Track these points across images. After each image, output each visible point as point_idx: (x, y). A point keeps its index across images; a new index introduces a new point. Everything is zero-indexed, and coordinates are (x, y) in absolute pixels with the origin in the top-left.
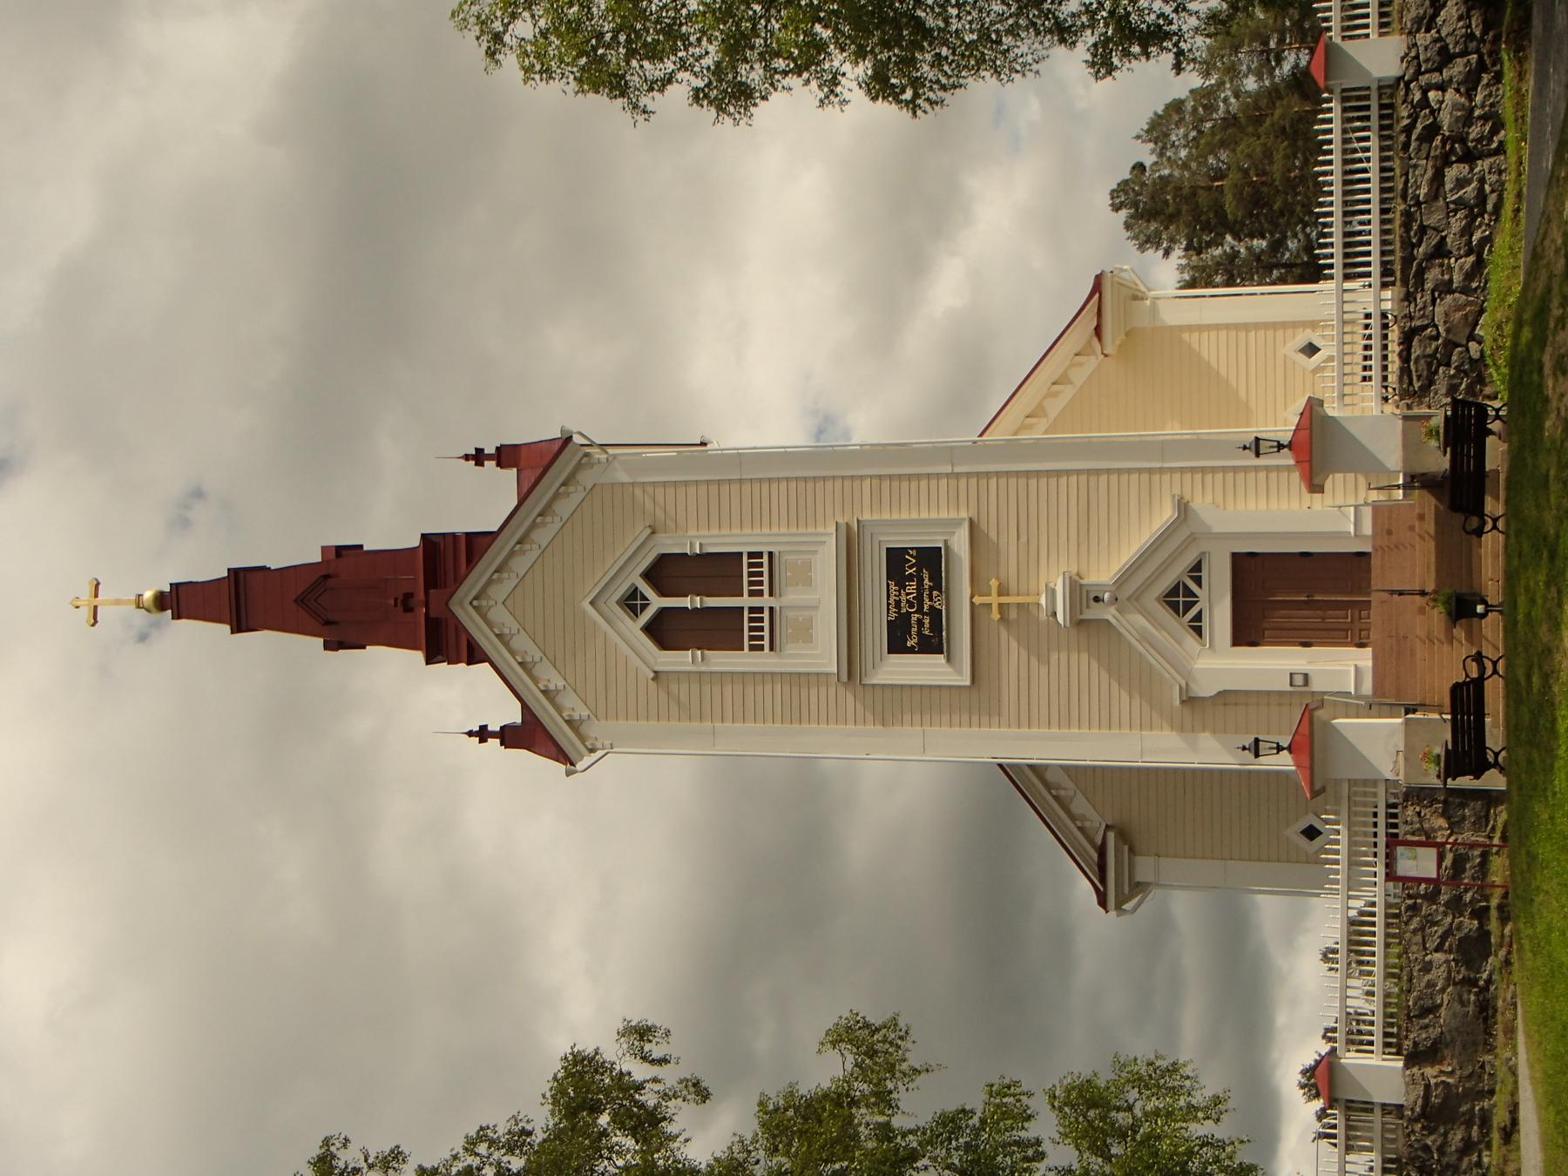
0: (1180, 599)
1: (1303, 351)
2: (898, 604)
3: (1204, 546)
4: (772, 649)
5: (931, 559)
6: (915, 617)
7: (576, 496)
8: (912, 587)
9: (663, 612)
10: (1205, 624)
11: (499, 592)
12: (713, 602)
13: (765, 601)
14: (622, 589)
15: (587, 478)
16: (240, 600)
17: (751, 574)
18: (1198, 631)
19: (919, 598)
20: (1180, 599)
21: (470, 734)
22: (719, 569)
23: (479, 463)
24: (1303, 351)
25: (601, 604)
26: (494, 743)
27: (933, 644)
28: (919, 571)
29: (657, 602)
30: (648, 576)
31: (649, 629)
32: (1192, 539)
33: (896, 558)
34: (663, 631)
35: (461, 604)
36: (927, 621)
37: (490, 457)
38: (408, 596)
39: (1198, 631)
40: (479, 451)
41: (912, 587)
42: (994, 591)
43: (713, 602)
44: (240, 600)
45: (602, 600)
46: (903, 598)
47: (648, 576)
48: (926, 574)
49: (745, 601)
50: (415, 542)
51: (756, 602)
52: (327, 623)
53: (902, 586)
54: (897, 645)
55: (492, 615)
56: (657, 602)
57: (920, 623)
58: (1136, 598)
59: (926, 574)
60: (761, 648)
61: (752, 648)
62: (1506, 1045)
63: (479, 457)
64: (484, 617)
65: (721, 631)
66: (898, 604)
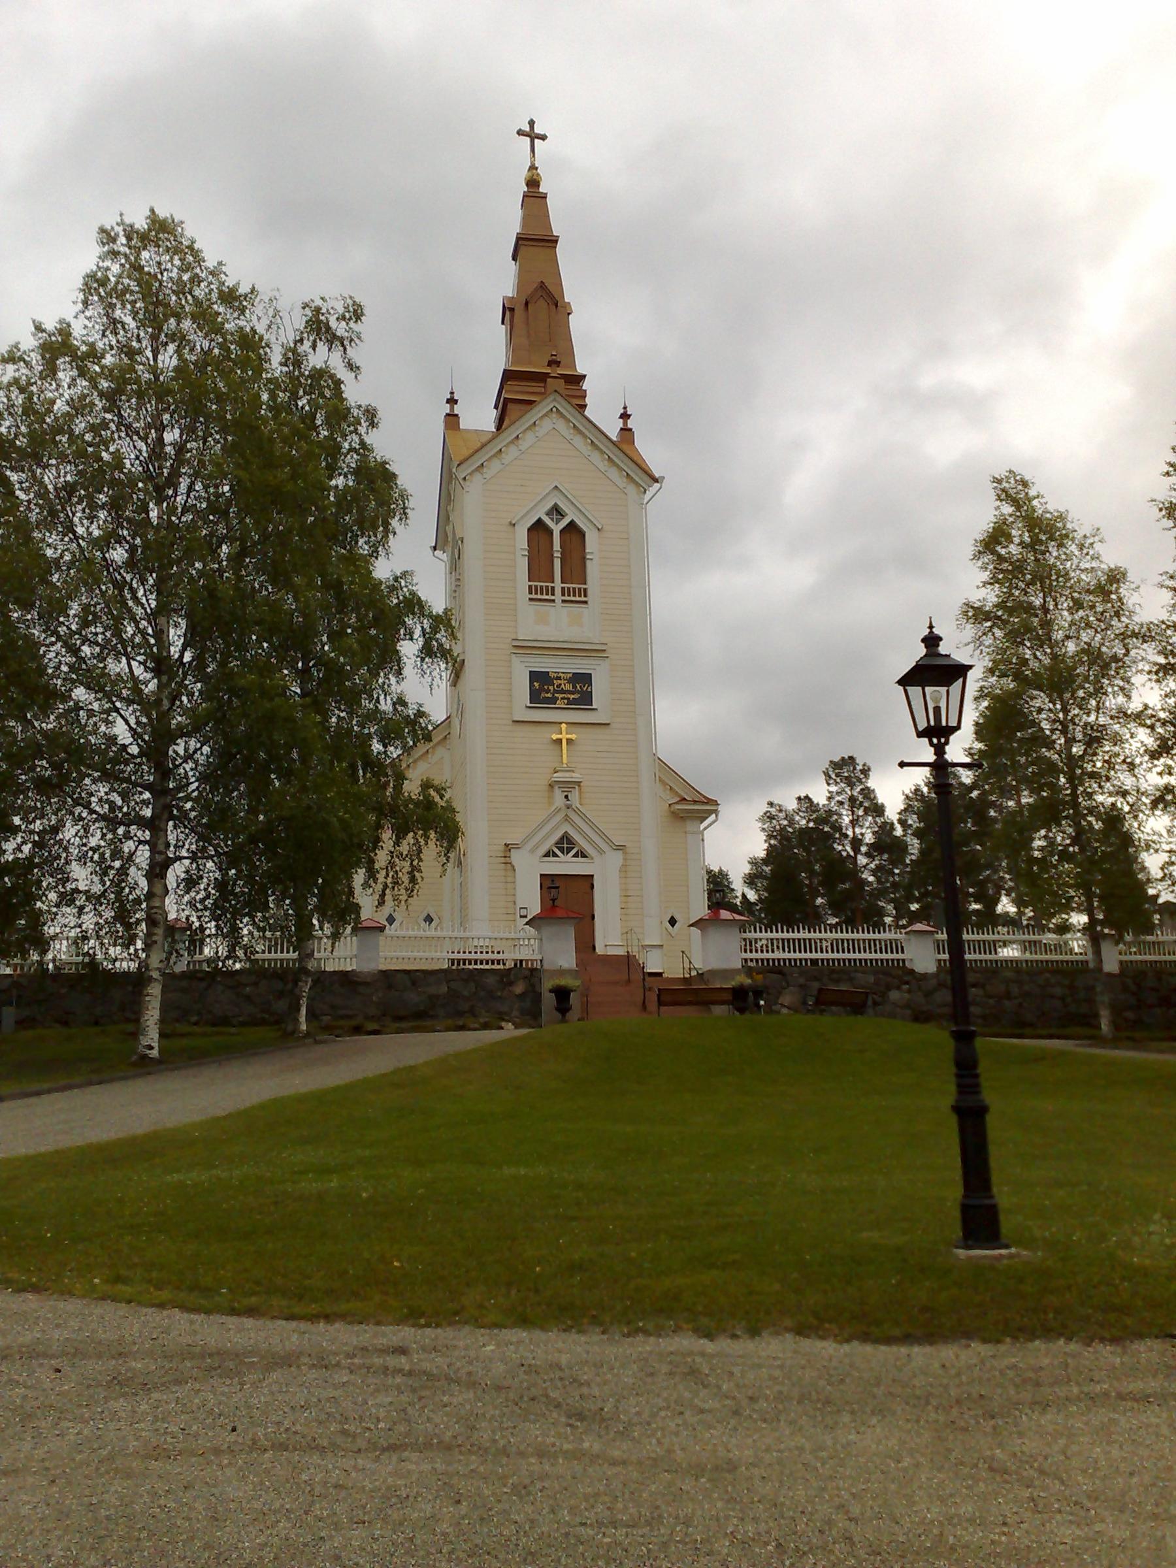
0: (566, 844)
1: (672, 918)
2: (559, 678)
3: (597, 859)
4: (530, 599)
5: (585, 700)
6: (551, 688)
7: (621, 481)
8: (569, 687)
9: (551, 532)
10: (551, 859)
11: (561, 425)
12: (557, 564)
13: (558, 596)
14: (563, 506)
15: (631, 489)
16: (536, 243)
17: (541, 587)
18: (547, 855)
19: (563, 692)
20: (566, 844)
21: (625, 408)
22: (576, 568)
23: (448, 401)
24: (672, 918)
25: (556, 492)
26: (620, 423)
27: (535, 697)
28: (578, 692)
29: (557, 529)
30: (572, 524)
31: (539, 522)
32: (601, 852)
33: (586, 679)
34: (538, 529)
35: (555, 400)
36: (549, 695)
37: (452, 409)
38: (558, 363)
39: (547, 855)
40: (456, 402)
41: (569, 687)
42: (569, 736)
43: (557, 564)
44: (536, 243)
45: (559, 494)
46: (562, 682)
47: (572, 524)
48: (576, 696)
49: (558, 585)
50: (580, 370)
51: (558, 591)
52: (527, 304)
53: (569, 681)
54: (534, 676)
55: (547, 421)
56: (557, 529)
57: (548, 691)
58: (567, 818)
59: (576, 696)
60: (530, 593)
61: (530, 587)
62: (851, 979)
63: (625, 416)
64: (546, 415)
65: (539, 567)
66: (559, 678)
